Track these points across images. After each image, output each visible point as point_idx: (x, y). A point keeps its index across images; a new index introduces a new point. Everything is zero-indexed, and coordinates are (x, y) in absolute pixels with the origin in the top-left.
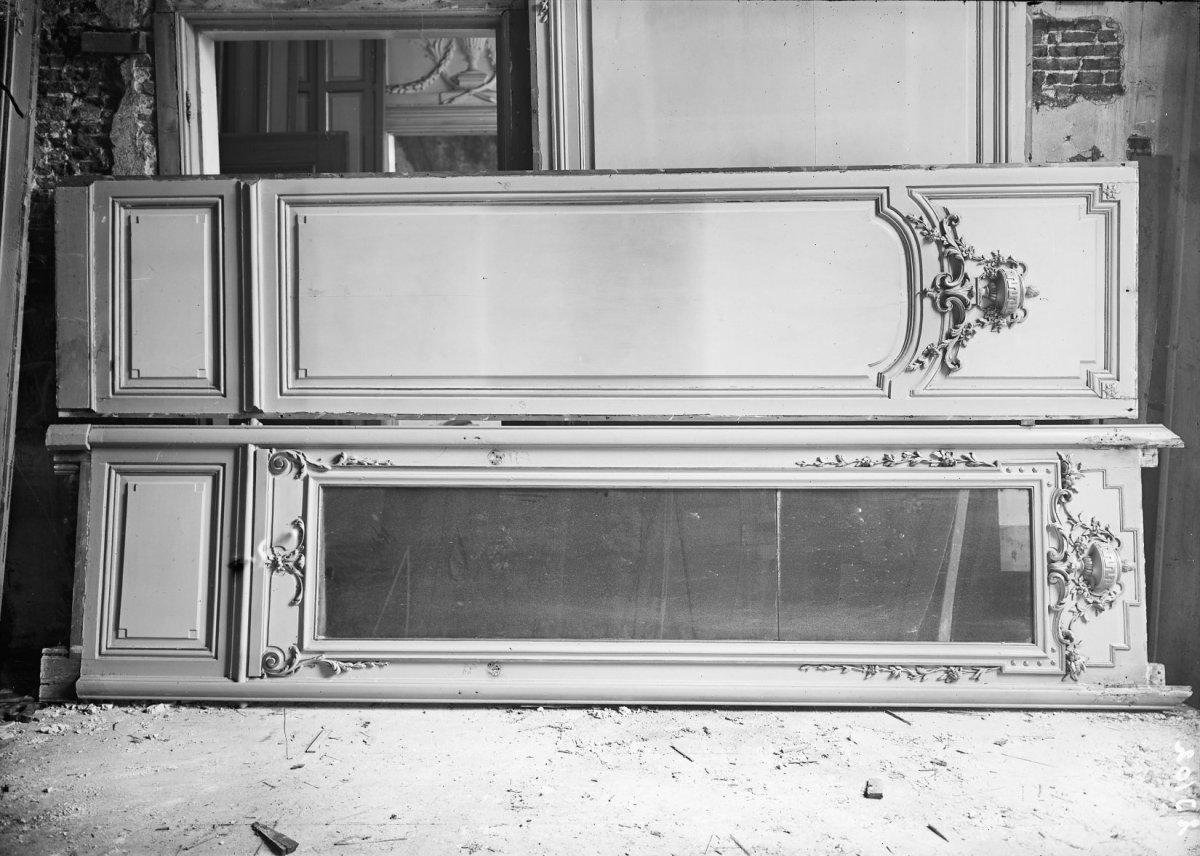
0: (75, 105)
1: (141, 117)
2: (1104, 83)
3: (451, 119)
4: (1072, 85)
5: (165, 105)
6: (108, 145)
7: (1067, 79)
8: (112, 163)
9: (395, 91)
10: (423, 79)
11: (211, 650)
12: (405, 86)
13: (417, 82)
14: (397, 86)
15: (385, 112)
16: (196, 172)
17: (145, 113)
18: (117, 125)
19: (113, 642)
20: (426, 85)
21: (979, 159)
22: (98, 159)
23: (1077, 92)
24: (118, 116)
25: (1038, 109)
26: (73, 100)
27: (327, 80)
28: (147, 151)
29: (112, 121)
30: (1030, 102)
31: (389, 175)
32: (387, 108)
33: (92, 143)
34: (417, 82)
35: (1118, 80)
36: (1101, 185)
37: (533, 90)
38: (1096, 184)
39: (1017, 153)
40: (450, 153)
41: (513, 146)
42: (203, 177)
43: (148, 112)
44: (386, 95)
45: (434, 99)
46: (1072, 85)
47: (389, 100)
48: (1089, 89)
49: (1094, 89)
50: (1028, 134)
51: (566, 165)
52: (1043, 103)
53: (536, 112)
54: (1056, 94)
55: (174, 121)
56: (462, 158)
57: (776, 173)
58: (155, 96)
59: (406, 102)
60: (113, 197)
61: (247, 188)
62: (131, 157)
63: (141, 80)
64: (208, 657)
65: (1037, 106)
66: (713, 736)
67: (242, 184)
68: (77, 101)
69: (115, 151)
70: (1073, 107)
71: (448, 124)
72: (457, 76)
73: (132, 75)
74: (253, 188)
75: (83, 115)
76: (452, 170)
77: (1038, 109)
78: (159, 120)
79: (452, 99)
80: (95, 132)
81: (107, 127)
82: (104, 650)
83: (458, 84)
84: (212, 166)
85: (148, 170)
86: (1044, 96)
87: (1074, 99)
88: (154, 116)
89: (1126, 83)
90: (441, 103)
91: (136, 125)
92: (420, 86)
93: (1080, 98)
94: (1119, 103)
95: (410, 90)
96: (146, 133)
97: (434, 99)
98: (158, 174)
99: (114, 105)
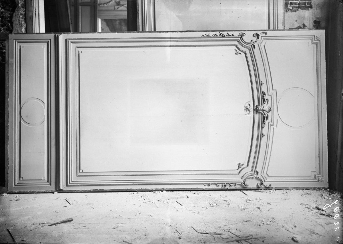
0: (2, 11)
1: (21, 14)
2: (306, 5)
3: (118, 14)
4: (297, 5)
5: (28, 11)
6: (12, 23)
7: (296, 4)
8: (13, 28)
9: (101, 6)
10: (109, 2)
11: (49, 183)
12: (104, 4)
13: (108, 3)
14: (101, 4)
15: (97, 12)
16: (38, 32)
17: (23, 13)
18: (14, 17)
19: (19, 181)
20: (110, 3)
21: (269, 28)
22: (9, 27)
23: (298, 7)
24: (14, 14)
25: (287, 12)
26: (1, 9)
27: (80, 2)
28: (23, 24)
29: (13, 16)
30: (284, 10)
31: (99, 33)
32: (99, 11)
33: (7, 22)
34: (108, 3)
35: (310, 4)
36: (315, 36)
37: (137, 7)
38: (313, 36)
39: (280, 27)
40: (120, 24)
41: (132, 23)
42: (39, 33)
43: (24, 13)
44: (98, 7)
45: (113, 8)
46: (297, 5)
47: (99, 8)
48: (302, 6)
49: (304, 7)
50: (284, 20)
51: (147, 30)
52: (288, 11)
53: (138, 13)
54: (293, 8)
55: (31, 16)
56: (124, 25)
57: (199, 32)
58: (25, 8)
59: (104, 9)
60: (15, 40)
61: (58, 37)
62: (18, 26)
63: (21, 3)
64: (48, 185)
65: (287, 11)
66: (189, 198)
67: (56, 35)
68: (2, 9)
69: (14, 25)
70: (297, 12)
71: (118, 15)
72: (119, 1)
73: (19, 2)
74: (60, 37)
75: (4, 14)
76: (120, 31)
77: (287, 12)
78: (27, 15)
79: (118, 8)
80: (8, 19)
81: (11, 17)
82: (16, 184)
83: (120, 3)
84: (43, 30)
85: (23, 30)
86: (289, 9)
87: (298, 10)
88: (25, 14)
89: (313, 5)
90: (115, 9)
91: (20, 17)
92: (108, 4)
93: (299, 9)
94: (311, 10)
95: (105, 5)
96: (23, 19)
97: (113, 8)
98: (27, 33)
99: (13, 11)
